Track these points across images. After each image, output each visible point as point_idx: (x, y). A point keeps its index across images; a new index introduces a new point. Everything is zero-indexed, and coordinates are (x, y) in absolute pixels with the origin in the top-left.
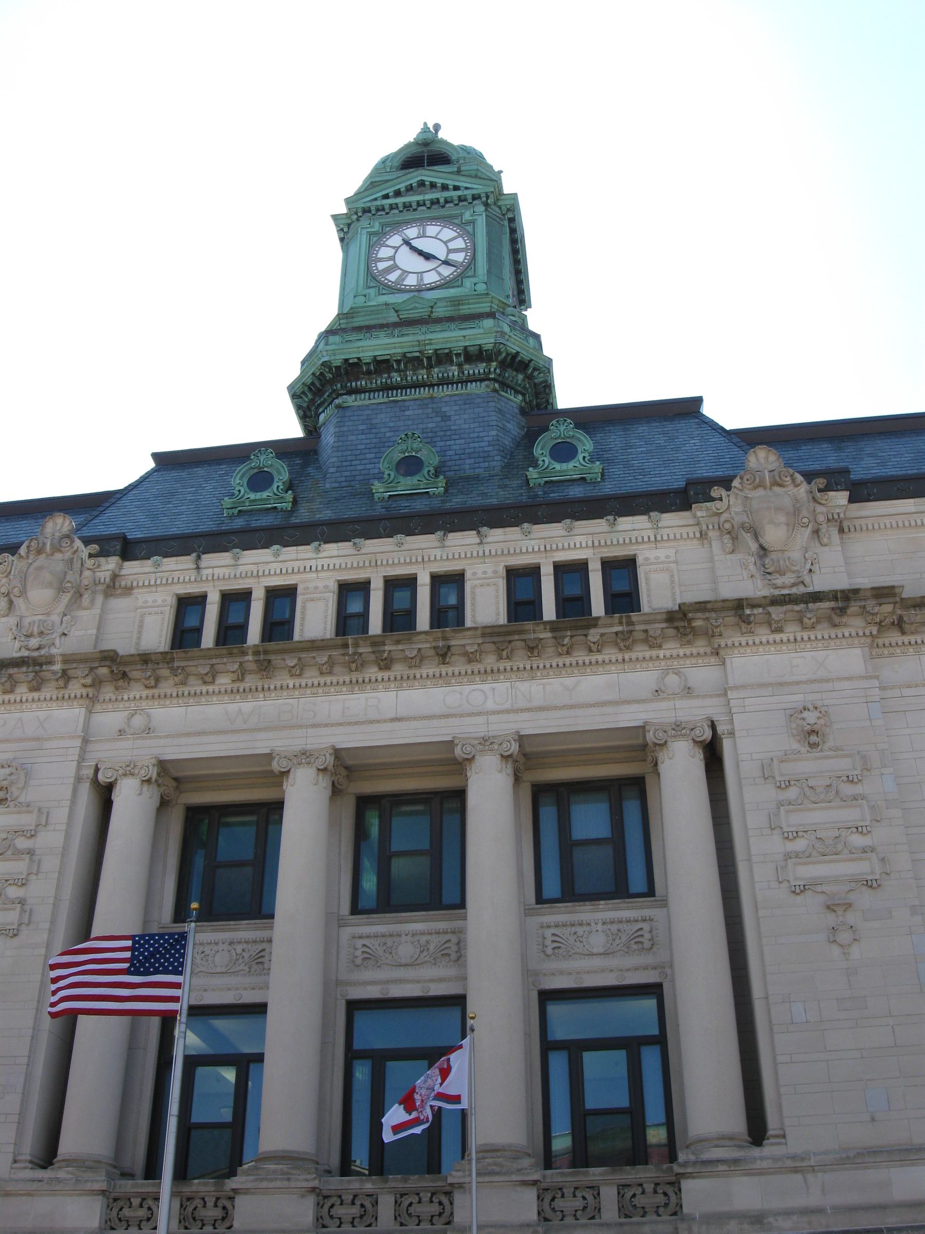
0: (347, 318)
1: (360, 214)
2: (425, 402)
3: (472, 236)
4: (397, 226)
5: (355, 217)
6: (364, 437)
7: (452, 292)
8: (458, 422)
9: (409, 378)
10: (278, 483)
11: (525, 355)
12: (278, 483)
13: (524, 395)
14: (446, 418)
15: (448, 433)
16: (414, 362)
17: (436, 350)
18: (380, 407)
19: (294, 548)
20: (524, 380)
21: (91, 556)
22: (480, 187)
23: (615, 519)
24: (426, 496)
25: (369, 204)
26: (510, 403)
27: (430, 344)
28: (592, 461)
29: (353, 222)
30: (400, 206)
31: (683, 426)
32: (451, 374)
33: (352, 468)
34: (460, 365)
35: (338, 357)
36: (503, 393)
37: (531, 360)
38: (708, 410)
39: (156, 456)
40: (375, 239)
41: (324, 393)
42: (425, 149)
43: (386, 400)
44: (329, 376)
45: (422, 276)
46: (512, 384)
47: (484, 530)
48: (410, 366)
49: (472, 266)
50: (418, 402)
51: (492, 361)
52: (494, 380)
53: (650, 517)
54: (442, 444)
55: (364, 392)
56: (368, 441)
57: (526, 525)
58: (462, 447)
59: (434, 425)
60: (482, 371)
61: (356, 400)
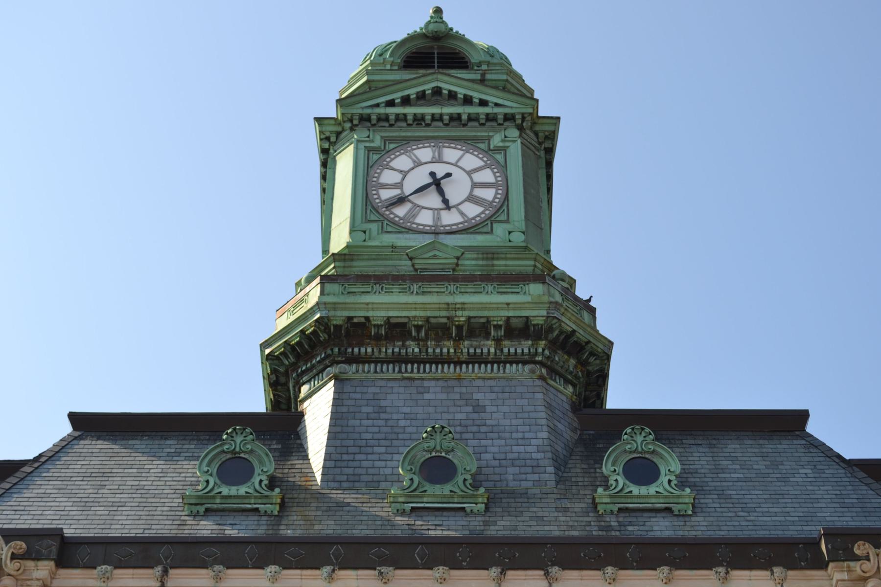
0: (345, 260)
1: (356, 122)
2: (450, 383)
3: (503, 168)
4: (405, 144)
5: (348, 125)
6: (370, 422)
7: (479, 240)
8: (495, 415)
9: (430, 350)
10: (259, 478)
11: (582, 335)
12: (259, 478)
13: (574, 386)
14: (479, 408)
15: (483, 429)
16: (439, 330)
17: (469, 318)
18: (390, 384)
19: (298, 572)
20: (575, 367)
21: (14, 557)
22: (515, 105)
23: (727, 573)
24: (462, 514)
25: (368, 111)
26: (560, 395)
27: (463, 309)
28: (681, 485)
29: (343, 130)
30: (410, 118)
31: (784, 446)
32: (485, 351)
33: (356, 464)
34: (498, 341)
35: (339, 313)
36: (552, 382)
37: (589, 342)
38: (811, 428)
39: (74, 417)
40: (376, 157)
41: (314, 357)
42: (435, 44)
43: (399, 376)
44: (323, 336)
45: (439, 214)
46: (562, 371)
47: (554, 570)
48: (432, 334)
49: (505, 208)
50: (440, 383)
51: (540, 339)
52: (541, 363)
53: (772, 573)
54: (475, 443)
55: (369, 362)
56: (376, 429)
57: (610, 570)
58: (503, 449)
59: (463, 416)
60: (526, 350)
61: (357, 371)
